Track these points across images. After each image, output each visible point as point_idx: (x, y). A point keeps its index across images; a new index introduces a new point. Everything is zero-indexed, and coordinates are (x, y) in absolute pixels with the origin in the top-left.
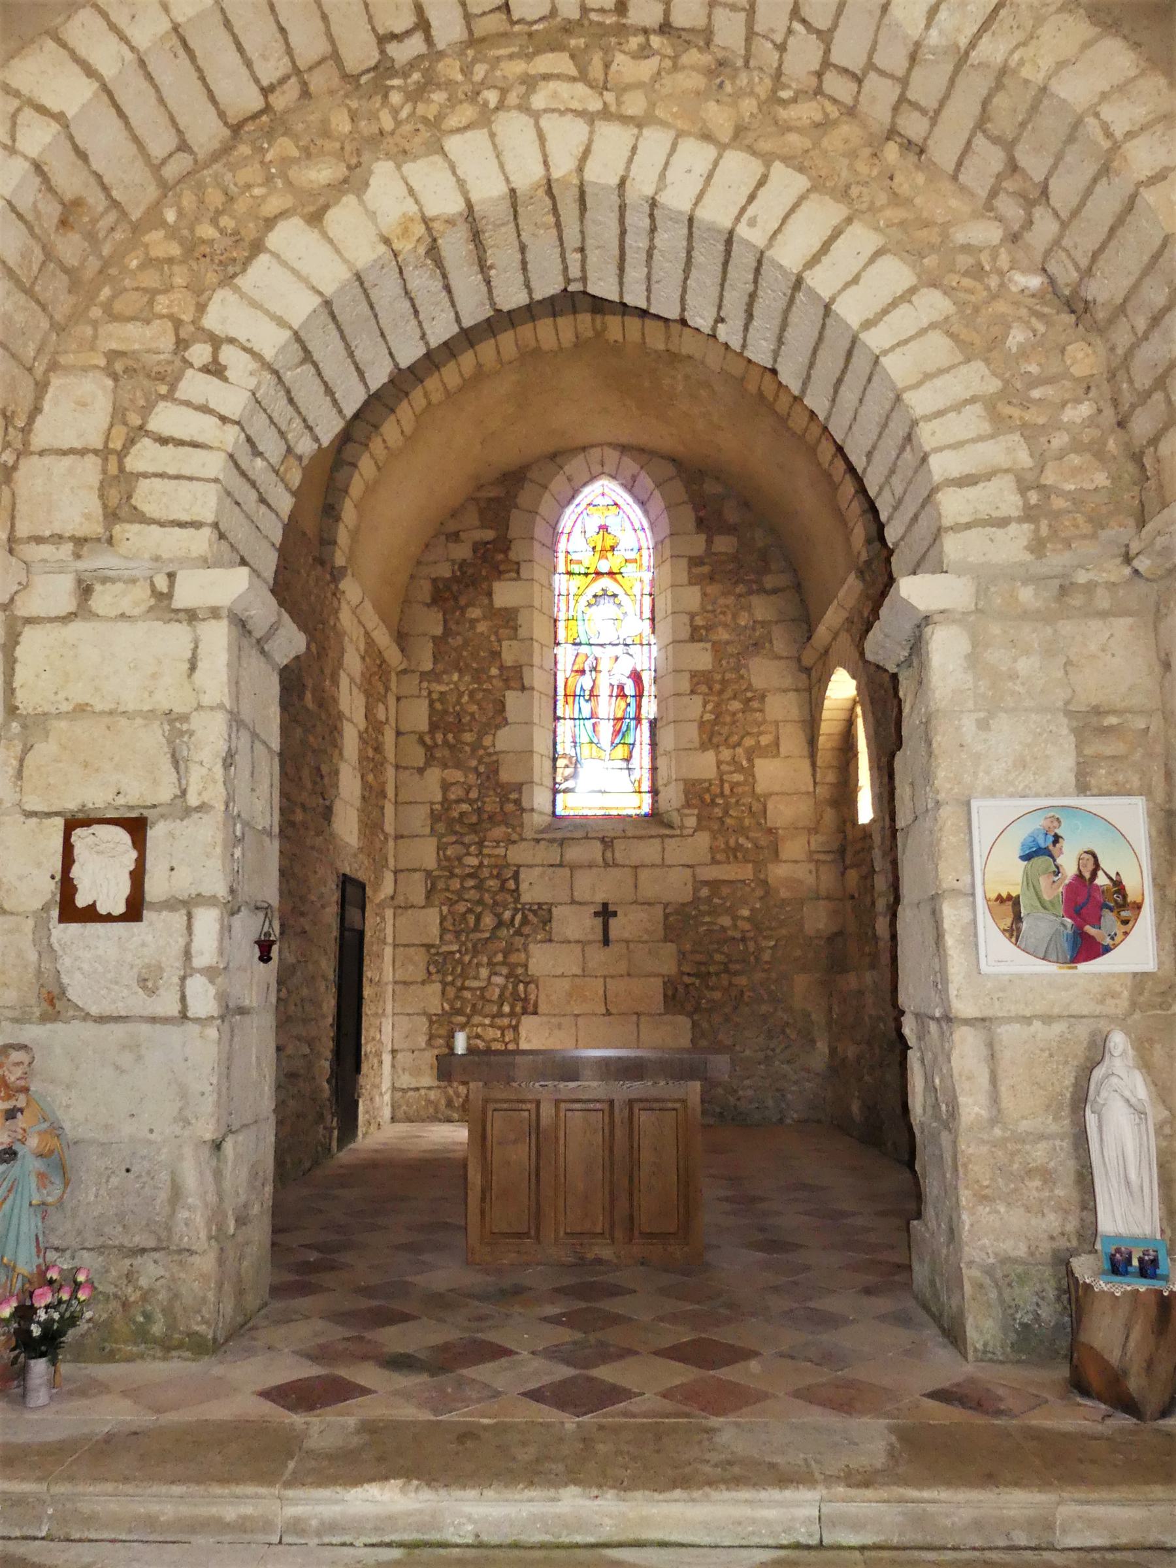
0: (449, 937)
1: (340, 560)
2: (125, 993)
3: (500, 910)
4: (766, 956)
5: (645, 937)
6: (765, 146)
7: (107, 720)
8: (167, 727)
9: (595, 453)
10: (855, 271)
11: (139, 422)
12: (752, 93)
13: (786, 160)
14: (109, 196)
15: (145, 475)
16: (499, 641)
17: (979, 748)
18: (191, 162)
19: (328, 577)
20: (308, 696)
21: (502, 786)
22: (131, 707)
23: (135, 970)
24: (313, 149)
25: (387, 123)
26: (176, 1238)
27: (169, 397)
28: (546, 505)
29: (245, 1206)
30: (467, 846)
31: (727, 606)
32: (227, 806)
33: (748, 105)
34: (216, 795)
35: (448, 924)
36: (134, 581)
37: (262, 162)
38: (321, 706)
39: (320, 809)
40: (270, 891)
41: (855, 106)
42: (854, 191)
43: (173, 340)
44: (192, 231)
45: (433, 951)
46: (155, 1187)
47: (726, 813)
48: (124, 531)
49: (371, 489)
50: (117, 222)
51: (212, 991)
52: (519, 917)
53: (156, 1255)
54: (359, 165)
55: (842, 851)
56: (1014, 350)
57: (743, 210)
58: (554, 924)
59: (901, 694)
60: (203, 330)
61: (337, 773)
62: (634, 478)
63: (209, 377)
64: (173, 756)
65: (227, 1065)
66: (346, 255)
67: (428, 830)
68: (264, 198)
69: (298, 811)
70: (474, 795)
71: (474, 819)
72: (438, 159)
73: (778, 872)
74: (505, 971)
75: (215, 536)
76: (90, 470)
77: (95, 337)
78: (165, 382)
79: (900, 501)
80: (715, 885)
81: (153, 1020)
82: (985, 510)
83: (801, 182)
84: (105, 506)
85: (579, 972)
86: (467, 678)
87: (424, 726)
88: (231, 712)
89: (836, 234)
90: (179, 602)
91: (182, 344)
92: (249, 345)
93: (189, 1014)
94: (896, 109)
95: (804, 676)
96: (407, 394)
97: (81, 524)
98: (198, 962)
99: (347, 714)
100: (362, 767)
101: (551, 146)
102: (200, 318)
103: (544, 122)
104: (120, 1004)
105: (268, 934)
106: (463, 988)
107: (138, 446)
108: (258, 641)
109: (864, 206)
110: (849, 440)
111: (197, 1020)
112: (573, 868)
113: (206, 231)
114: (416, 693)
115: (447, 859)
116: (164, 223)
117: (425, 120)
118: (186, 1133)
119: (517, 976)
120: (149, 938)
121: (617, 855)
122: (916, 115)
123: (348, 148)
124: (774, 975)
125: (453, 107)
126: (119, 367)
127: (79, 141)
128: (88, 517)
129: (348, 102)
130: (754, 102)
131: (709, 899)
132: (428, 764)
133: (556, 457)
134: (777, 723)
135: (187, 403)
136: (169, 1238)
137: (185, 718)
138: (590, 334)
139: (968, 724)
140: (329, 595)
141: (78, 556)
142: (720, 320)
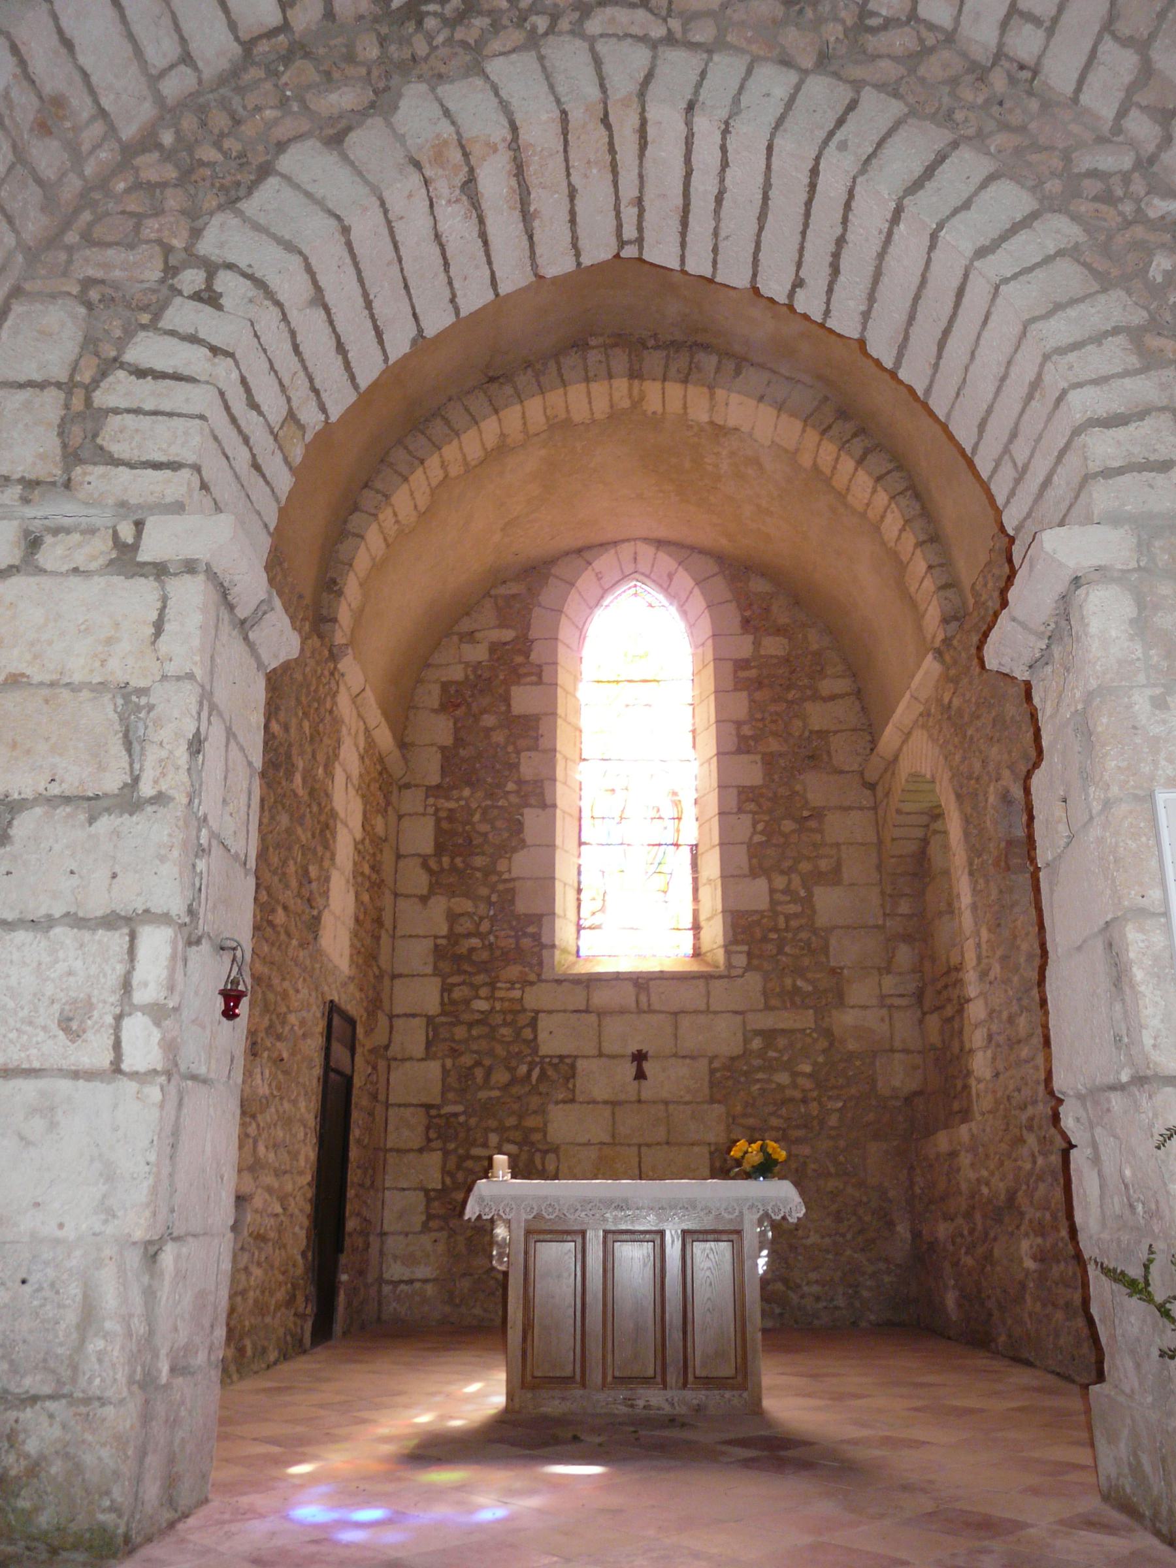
0: (451, 1096)
1: (340, 638)
2: (42, 1035)
3: (514, 1063)
4: (833, 1120)
5: (688, 1098)
6: (857, 72)
7: (45, 692)
8: (120, 701)
9: (626, 550)
10: (965, 196)
11: (113, 354)
12: (837, 19)
13: (880, 87)
14: (96, 102)
15: (116, 411)
16: (518, 752)
17: (1156, 730)
18: (195, 81)
19: (326, 653)
20: (298, 779)
21: (518, 917)
22: (77, 678)
23: (57, 1007)
24: (336, 75)
25: (421, 48)
26: (82, 1382)
27: (152, 326)
28: (572, 605)
29: (186, 1348)
30: (475, 988)
31: (777, 713)
32: (190, 802)
33: (833, 32)
34: (176, 783)
35: (452, 1080)
36: (92, 531)
37: (276, 86)
38: (312, 793)
39: (306, 917)
40: (240, 924)
41: (955, 29)
42: (959, 116)
43: (161, 266)
44: (191, 155)
45: (433, 1112)
46: (60, 1306)
47: (780, 951)
48: (85, 474)
49: (378, 567)
50: (104, 138)
51: (156, 1035)
52: (536, 1073)
53: (50, 1405)
54: (387, 89)
55: (919, 996)
56: (1159, 279)
57: (831, 134)
58: (579, 1082)
59: (1036, 700)
60: (197, 257)
61: (327, 879)
62: (670, 576)
63: (200, 306)
64: (126, 735)
65: (173, 1139)
66: (370, 177)
67: (429, 970)
68: (276, 122)
69: (280, 911)
70: (485, 926)
71: (485, 955)
72: (479, 82)
73: (845, 1019)
74: (517, 1135)
75: (196, 483)
76: (51, 404)
77: (69, 262)
78: (149, 313)
79: (1025, 468)
80: (769, 1036)
81: (76, 1075)
82: (1139, 454)
83: (896, 108)
84: (65, 446)
85: (606, 1138)
86: (480, 794)
87: (428, 848)
88: (202, 687)
89: (941, 158)
90: (144, 556)
91: (171, 271)
92: (250, 271)
93: (125, 1067)
94: (1004, 25)
95: (868, 792)
96: (422, 462)
97: (34, 464)
98: (141, 996)
99: (342, 814)
100: (356, 884)
101: (608, 68)
102: (193, 245)
103: (602, 47)
104: (34, 1051)
105: (235, 982)
106: (468, 1157)
107: (111, 379)
108: (243, 622)
109: (971, 132)
110: (956, 413)
111: (134, 1075)
112: (601, 1014)
113: (208, 153)
114: (421, 810)
115: (453, 1002)
116: (159, 146)
117: (464, 44)
118: (110, 1229)
119: (533, 1144)
120: (78, 965)
121: (654, 998)
122: (1028, 28)
123: (375, 73)
124: (842, 1143)
125: (497, 32)
126: (94, 295)
127: (64, 23)
128: (42, 457)
129: (377, 26)
130: (840, 28)
131: (762, 1054)
132: (432, 892)
133: (583, 553)
134: (838, 845)
135: (172, 333)
136: (74, 1380)
137: (143, 692)
138: (626, 403)
139: (1141, 702)
140: (326, 673)
141: (26, 501)
142: (798, 283)
